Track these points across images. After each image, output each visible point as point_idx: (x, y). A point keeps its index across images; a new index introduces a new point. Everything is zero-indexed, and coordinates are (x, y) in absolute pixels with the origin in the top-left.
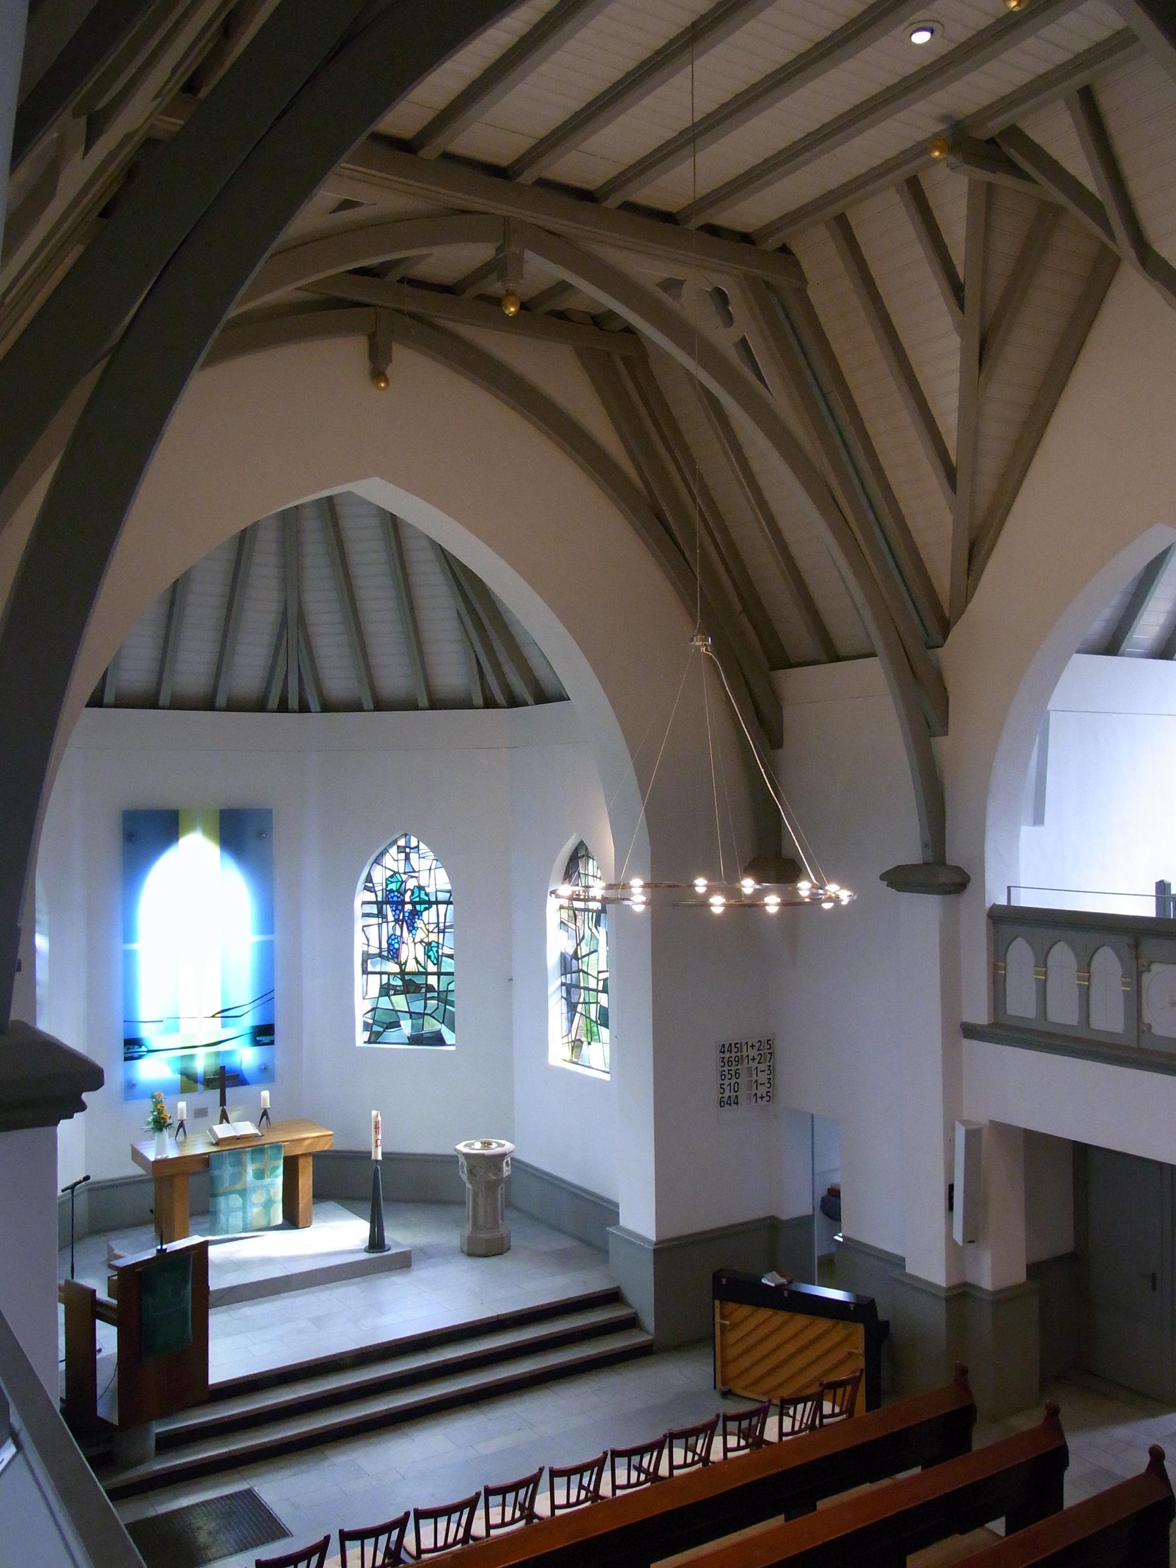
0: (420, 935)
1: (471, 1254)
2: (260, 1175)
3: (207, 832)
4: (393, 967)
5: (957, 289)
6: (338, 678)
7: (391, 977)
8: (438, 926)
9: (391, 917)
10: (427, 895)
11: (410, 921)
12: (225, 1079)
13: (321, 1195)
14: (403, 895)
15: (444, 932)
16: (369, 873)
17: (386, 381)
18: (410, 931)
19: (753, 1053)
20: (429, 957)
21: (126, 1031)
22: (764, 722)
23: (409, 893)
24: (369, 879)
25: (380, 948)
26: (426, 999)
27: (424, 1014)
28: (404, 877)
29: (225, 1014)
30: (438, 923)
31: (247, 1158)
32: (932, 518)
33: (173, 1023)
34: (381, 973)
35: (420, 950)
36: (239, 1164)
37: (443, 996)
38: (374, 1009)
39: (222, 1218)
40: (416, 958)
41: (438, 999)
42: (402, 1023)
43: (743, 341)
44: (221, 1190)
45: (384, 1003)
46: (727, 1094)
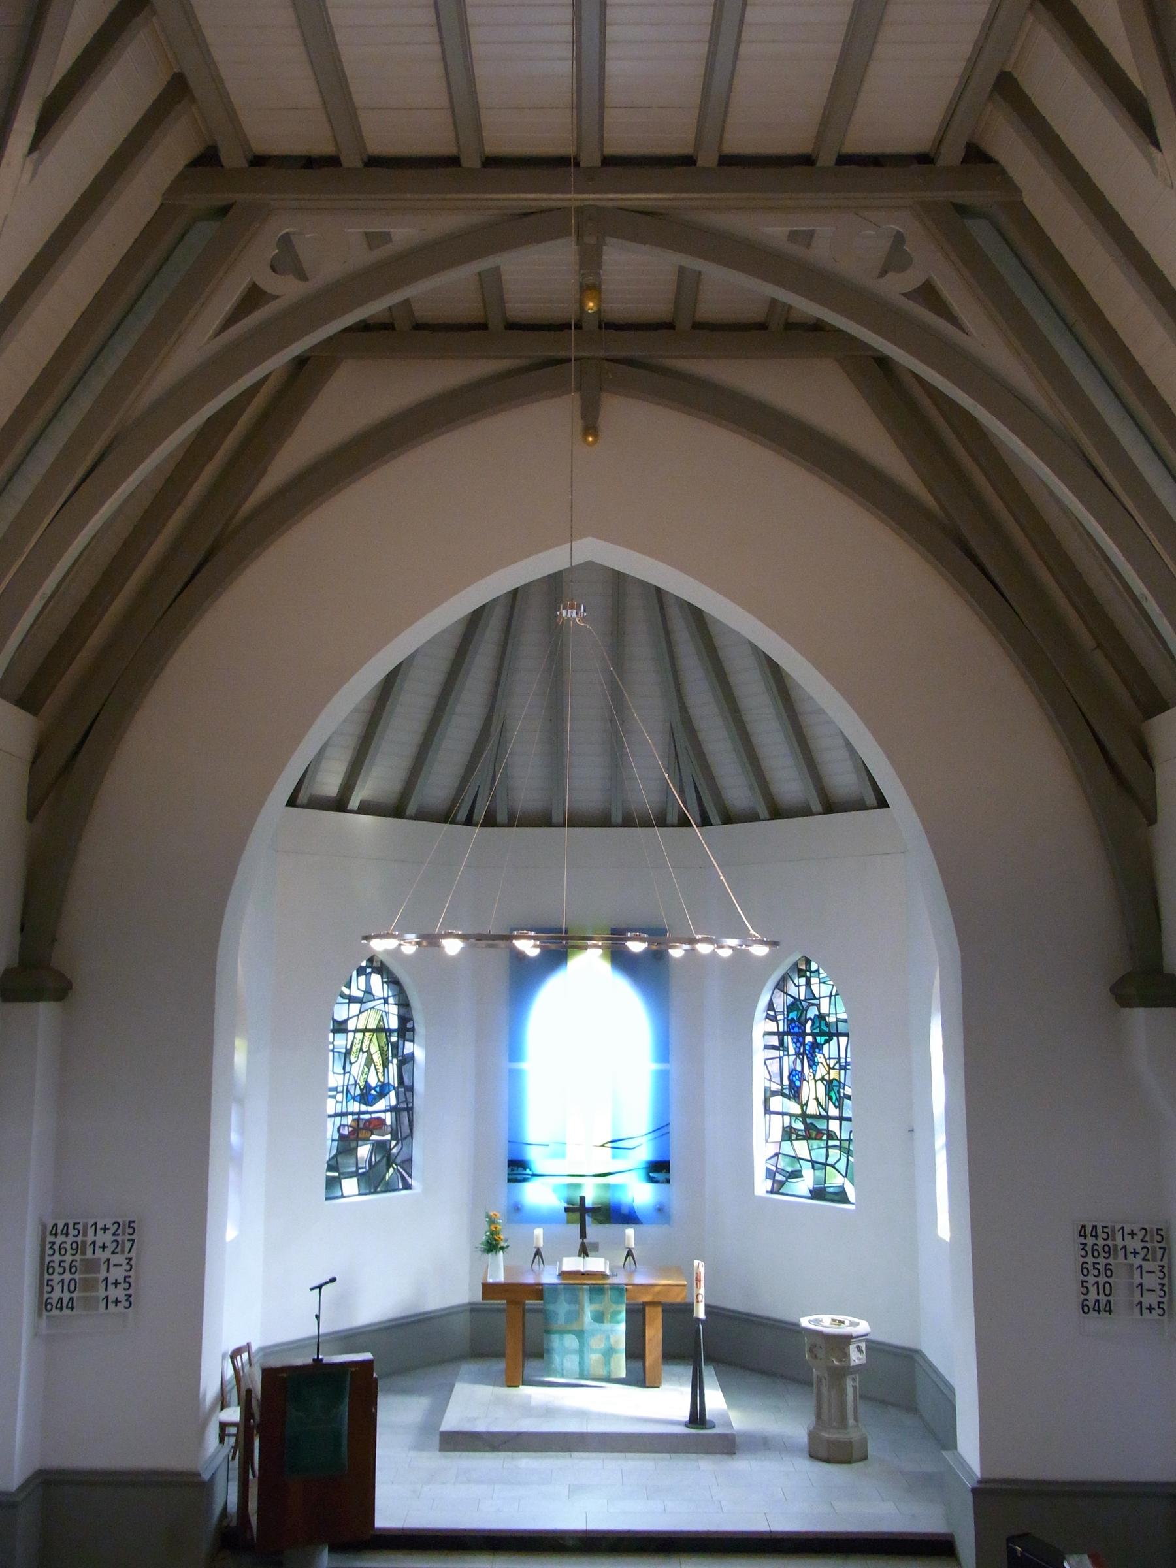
0: (821, 1071)
1: (814, 1456)
2: (599, 1318)
6: (737, 789)
7: (793, 1119)
8: (839, 1062)
9: (792, 1051)
10: (827, 1025)
11: (809, 1054)
12: (614, 1214)
13: (670, 1356)
15: (845, 1069)
17: (596, 436)
18: (810, 1067)
20: (831, 1098)
21: (510, 1151)
23: (810, 1023)
25: (782, 1084)
26: (828, 1147)
27: (826, 1164)
30: (839, 1058)
31: (586, 1297)
34: (783, 1114)
35: (821, 1087)
36: (575, 1300)
37: (845, 1144)
38: (777, 1155)
39: (557, 1359)
40: (817, 1099)
41: (840, 1148)
42: (803, 1172)
44: (555, 1327)
45: (787, 1148)
46: (1093, 1296)
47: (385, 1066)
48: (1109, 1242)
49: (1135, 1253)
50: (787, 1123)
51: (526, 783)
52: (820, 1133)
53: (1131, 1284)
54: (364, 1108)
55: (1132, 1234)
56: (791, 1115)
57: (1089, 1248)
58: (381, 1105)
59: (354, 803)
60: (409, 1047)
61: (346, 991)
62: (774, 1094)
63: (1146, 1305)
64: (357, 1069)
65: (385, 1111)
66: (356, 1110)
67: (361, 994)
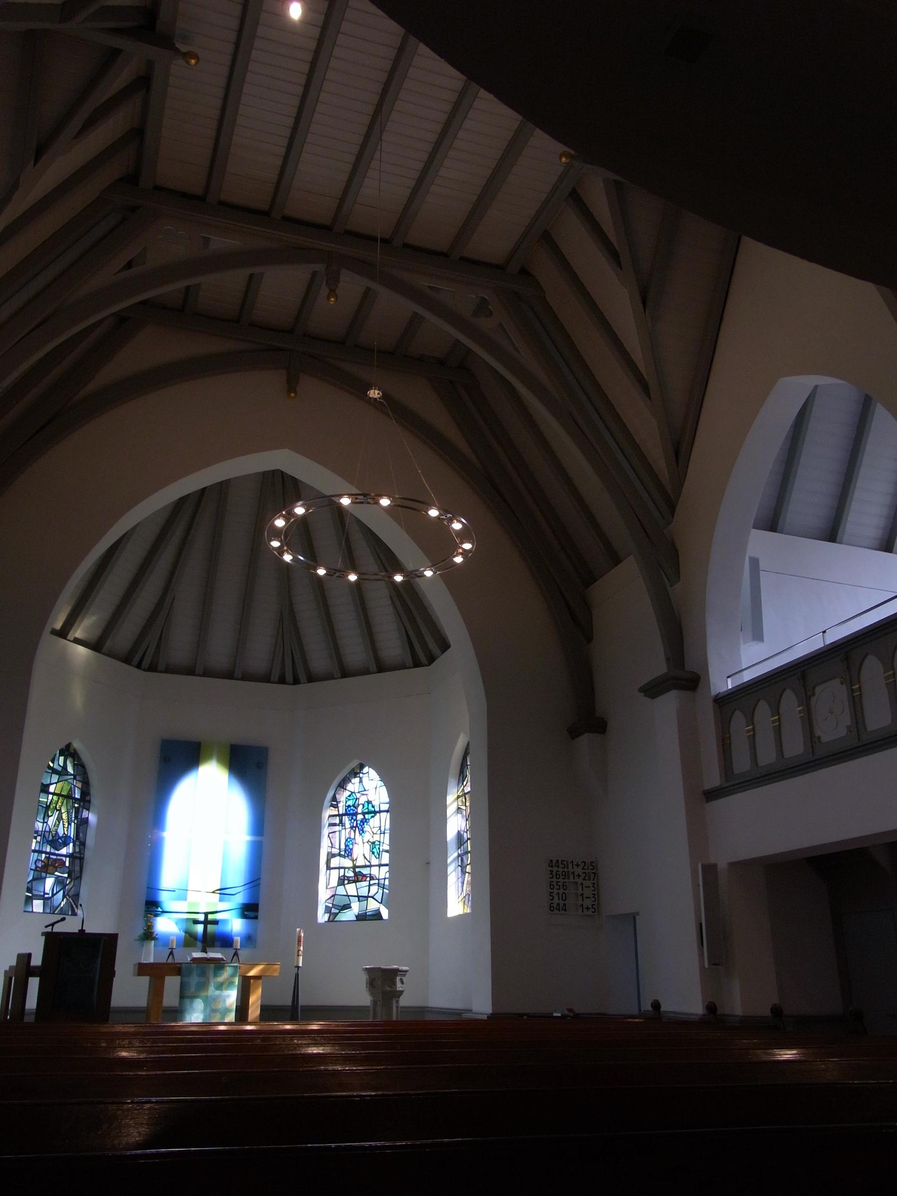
0: (367, 836)
3: (221, 761)
4: (347, 863)
5: (614, 256)
9: (348, 825)
10: (373, 807)
11: (359, 827)
14: (356, 808)
16: (335, 795)
17: (296, 393)
19: (579, 870)
20: (373, 853)
22: (575, 623)
23: (361, 807)
24: (334, 798)
28: (358, 795)
29: (222, 892)
32: (646, 428)
33: (182, 894)
34: (339, 868)
35: (367, 847)
37: (382, 882)
38: (333, 896)
42: (352, 905)
43: (501, 325)
45: (341, 890)
47: (69, 824)
48: (565, 870)
49: (579, 876)
50: (342, 873)
51: (180, 643)
52: (364, 876)
53: (577, 894)
54: (53, 851)
55: (578, 865)
56: (345, 868)
57: (554, 873)
58: (64, 851)
59: (71, 636)
60: (85, 814)
61: (51, 765)
62: (334, 856)
63: (585, 906)
64: (51, 821)
65: (66, 856)
66: (48, 850)
67: (60, 769)
